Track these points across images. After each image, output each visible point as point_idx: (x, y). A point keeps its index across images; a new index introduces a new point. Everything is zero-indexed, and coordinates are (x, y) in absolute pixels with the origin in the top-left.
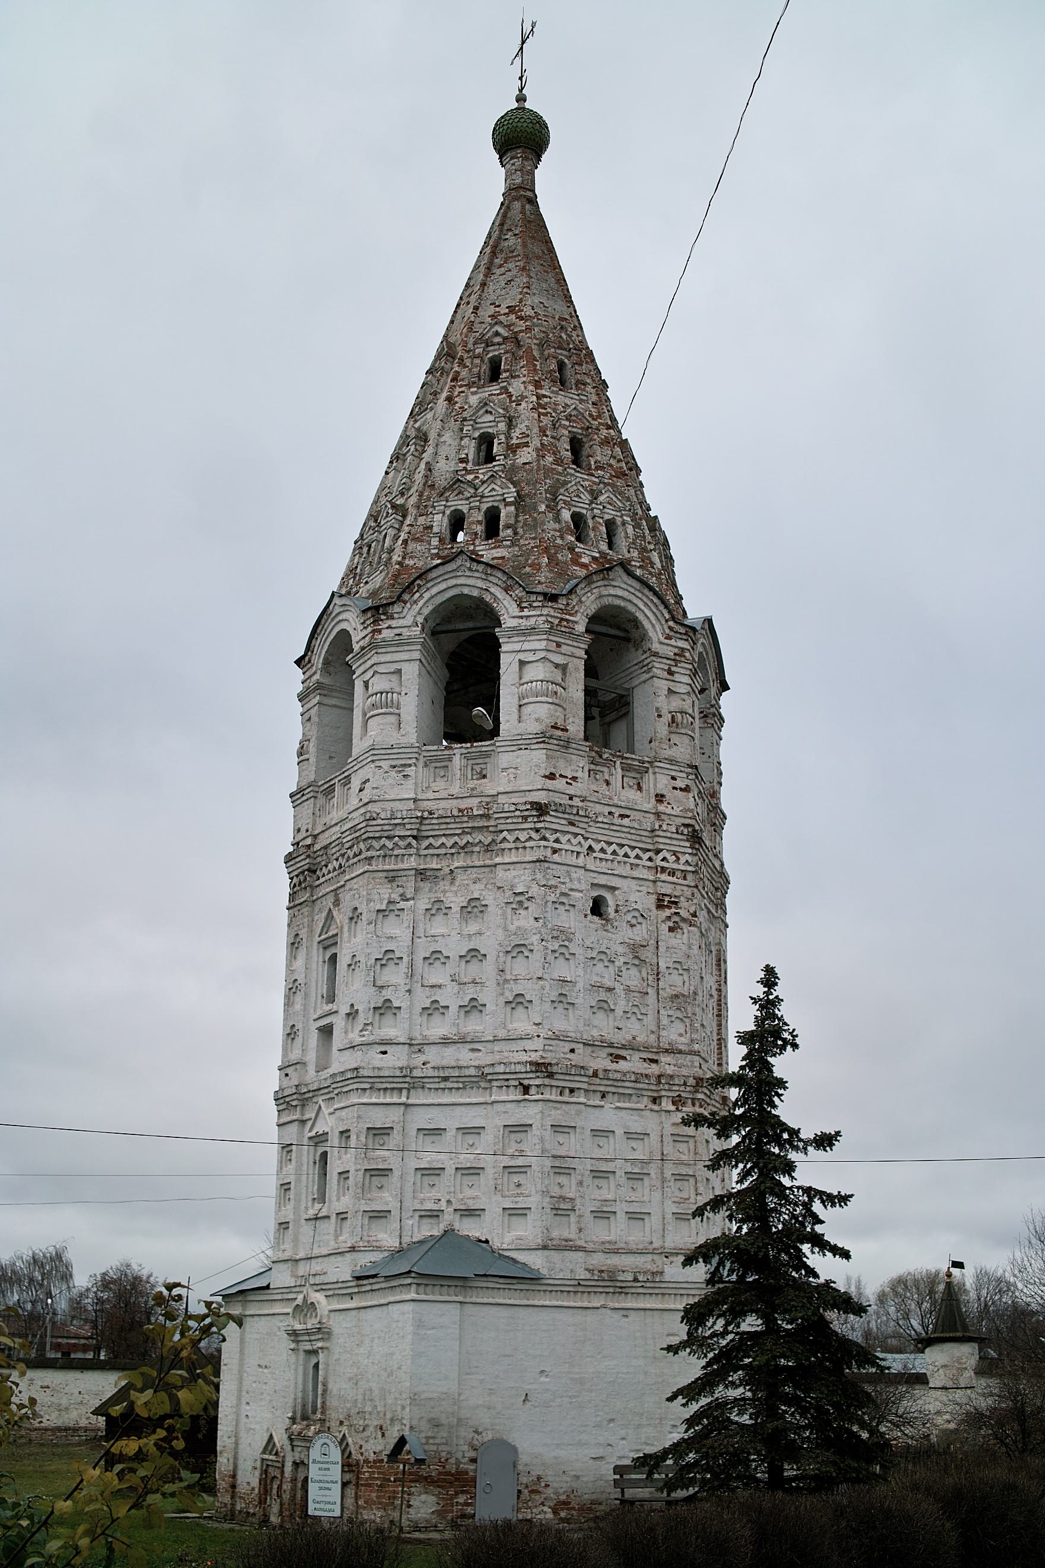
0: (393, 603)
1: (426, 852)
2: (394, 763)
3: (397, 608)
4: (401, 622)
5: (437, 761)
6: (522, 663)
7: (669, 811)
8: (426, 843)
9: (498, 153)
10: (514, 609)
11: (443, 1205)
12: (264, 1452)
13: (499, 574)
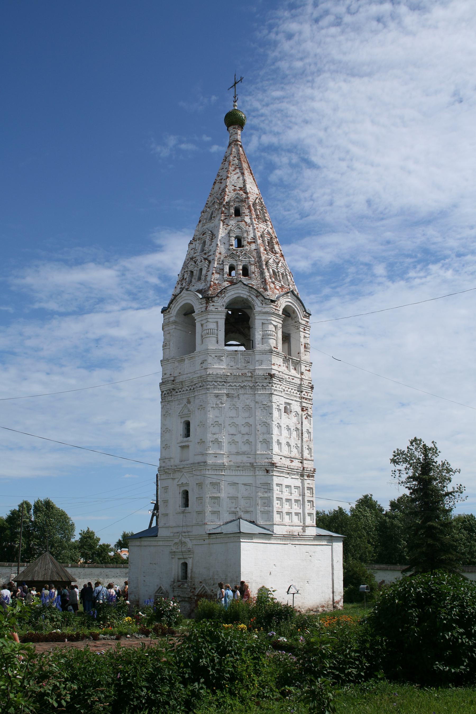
0: (214, 297)
1: (229, 388)
2: (216, 355)
3: (216, 299)
4: (217, 304)
5: (231, 355)
6: (263, 323)
7: (305, 378)
8: (229, 384)
9: (227, 126)
10: (259, 304)
11: (238, 509)
12: (156, 593)
13: (255, 291)
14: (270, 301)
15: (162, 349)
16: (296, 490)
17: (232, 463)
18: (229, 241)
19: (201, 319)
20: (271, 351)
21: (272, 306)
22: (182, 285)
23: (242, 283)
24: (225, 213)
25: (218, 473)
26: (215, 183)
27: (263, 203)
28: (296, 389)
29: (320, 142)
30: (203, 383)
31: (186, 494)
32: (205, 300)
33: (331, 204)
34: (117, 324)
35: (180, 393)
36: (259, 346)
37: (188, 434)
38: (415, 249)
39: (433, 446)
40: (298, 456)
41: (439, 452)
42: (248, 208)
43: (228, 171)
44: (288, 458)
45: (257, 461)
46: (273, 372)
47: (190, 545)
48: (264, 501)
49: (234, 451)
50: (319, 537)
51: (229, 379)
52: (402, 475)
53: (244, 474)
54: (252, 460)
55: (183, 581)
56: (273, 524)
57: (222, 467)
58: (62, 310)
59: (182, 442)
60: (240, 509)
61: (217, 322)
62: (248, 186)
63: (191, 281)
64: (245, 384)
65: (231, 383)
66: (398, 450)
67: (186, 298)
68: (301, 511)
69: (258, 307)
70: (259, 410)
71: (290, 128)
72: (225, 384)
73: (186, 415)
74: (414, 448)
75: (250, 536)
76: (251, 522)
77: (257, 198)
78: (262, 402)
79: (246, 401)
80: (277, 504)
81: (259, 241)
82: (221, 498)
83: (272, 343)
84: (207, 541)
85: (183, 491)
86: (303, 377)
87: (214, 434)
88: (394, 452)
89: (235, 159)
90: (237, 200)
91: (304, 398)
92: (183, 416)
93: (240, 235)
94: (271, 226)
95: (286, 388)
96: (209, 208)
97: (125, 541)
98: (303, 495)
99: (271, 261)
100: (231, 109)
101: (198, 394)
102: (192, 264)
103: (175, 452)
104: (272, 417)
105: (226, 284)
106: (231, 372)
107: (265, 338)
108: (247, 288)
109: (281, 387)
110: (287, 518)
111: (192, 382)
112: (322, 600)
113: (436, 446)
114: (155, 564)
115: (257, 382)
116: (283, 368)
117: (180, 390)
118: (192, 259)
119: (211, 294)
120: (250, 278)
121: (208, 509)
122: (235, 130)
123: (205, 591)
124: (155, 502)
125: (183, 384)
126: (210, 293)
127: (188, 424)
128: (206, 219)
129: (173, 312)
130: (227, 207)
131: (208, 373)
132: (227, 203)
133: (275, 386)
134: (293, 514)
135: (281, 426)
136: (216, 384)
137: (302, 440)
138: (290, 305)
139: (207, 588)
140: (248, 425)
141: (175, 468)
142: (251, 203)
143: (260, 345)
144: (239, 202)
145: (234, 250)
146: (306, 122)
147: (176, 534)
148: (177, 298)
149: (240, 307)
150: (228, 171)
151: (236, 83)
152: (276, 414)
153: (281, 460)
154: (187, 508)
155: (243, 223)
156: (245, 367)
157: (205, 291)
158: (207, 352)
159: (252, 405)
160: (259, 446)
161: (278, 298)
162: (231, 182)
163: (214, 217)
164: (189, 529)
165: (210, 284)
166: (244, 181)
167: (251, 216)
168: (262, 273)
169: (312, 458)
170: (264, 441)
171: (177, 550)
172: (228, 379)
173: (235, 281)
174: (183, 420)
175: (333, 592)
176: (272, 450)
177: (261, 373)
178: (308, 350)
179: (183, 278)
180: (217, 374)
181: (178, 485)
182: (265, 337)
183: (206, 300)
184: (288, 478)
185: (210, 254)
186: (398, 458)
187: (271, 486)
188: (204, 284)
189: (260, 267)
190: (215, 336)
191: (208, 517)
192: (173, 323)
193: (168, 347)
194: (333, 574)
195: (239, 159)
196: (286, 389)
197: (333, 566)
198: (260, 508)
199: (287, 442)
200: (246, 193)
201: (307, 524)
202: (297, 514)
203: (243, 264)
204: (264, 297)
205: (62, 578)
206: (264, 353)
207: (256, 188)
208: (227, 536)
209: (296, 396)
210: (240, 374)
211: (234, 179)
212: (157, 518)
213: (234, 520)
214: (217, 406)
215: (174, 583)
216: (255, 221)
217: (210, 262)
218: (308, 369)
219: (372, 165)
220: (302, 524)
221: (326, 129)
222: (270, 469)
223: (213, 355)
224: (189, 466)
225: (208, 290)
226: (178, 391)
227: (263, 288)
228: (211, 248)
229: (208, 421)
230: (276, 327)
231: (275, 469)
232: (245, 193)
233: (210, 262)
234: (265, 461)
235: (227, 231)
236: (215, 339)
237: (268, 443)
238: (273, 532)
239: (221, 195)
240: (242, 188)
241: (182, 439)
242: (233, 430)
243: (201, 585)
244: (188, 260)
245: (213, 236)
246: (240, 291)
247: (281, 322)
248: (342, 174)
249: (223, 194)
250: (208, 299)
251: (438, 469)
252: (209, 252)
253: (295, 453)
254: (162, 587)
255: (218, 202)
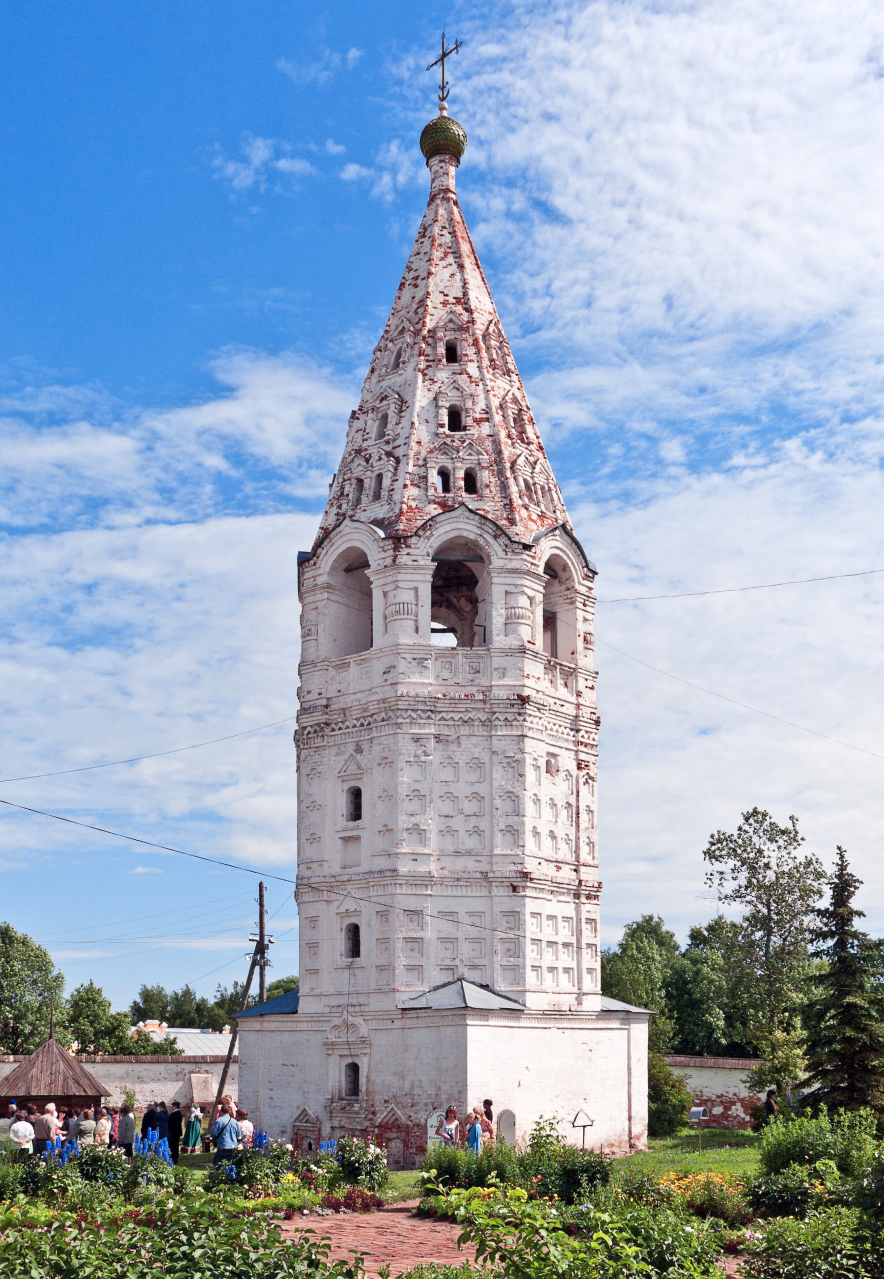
0: (411, 536)
1: (440, 722)
3: (414, 540)
4: (417, 552)
6: (507, 593)
8: (439, 716)
9: (425, 155)
10: (501, 554)
11: (457, 962)
13: (491, 526)
14: (521, 547)
15: (300, 641)
16: (566, 924)
17: (446, 873)
18: (437, 416)
19: (382, 582)
20: (523, 650)
21: (524, 557)
22: (340, 507)
23: (467, 507)
24: (428, 355)
25: (419, 892)
26: (402, 285)
27: (503, 332)
28: (568, 725)
29: (576, 163)
30: (388, 713)
31: (354, 932)
32: (391, 542)
33: (589, 303)
34: (132, 552)
35: (341, 732)
36: (499, 640)
37: (356, 813)
38: (757, 403)
39: (791, 828)
40: (571, 859)
41: (803, 839)
42: (473, 345)
43: (429, 260)
44: (552, 861)
45: (495, 869)
46: (526, 692)
47: (364, 1030)
48: (507, 946)
49: (450, 847)
50: (606, 1013)
51: (440, 706)
52: (725, 883)
53: (469, 894)
54: (484, 867)
55: (349, 1098)
56: (525, 991)
57: (427, 880)
58: (18, 521)
59: (344, 830)
60: (462, 961)
61: (416, 589)
62: (472, 295)
63: (358, 501)
64: (471, 715)
65: (443, 714)
66: (719, 832)
67: (352, 536)
68: (573, 965)
69: (498, 557)
70: (500, 768)
71: (513, 130)
72: (433, 716)
73: (354, 777)
74: (751, 830)
75: (485, 1013)
76: (482, 986)
77: (491, 322)
78: (504, 752)
79: (473, 749)
80: (533, 951)
81: (498, 418)
82: (426, 941)
83: (525, 632)
84: (398, 1024)
85: (349, 925)
86: (581, 701)
87: (412, 815)
88: (712, 836)
89: (445, 232)
90: (451, 325)
91: (582, 743)
92: (346, 778)
93: (458, 403)
94: (518, 384)
95: (549, 723)
96: (392, 341)
97: (149, 1006)
98: (579, 932)
99: (521, 461)
100: (435, 115)
101: (379, 734)
102: (359, 465)
103: (331, 851)
104: (524, 783)
105: (433, 510)
106: (444, 691)
107: (511, 621)
108: (477, 518)
109: (540, 722)
110: (548, 976)
111: (365, 710)
112: (611, 1133)
113: (798, 828)
114: (293, 1065)
115: (495, 713)
116: (544, 685)
117: (340, 725)
118: (358, 451)
119: (404, 530)
120: (481, 497)
121: (401, 961)
122: (443, 164)
123: (394, 1118)
124: (257, 938)
125: (347, 713)
126: (401, 526)
127: (356, 795)
128: (387, 366)
129: (323, 565)
130: (430, 341)
131: (399, 694)
132: (429, 331)
133: (529, 719)
134: (561, 970)
135: (539, 800)
136: (414, 715)
137: (578, 826)
138: (558, 555)
139: (399, 1112)
140: (477, 796)
141: (333, 880)
142: (479, 334)
143: (502, 637)
144: (454, 330)
145: (447, 436)
146: (549, 117)
147: (335, 1010)
148: (331, 536)
149: (461, 558)
150: (429, 260)
151: (444, 55)
152: (530, 775)
153: (539, 867)
154: (358, 959)
155: (465, 376)
156: (472, 681)
157: (390, 524)
158: (396, 649)
159: (485, 757)
160: (499, 838)
161: (537, 540)
162: (436, 285)
163: (404, 363)
164: (362, 1000)
165: (401, 509)
166: (465, 283)
167: (480, 361)
168: (504, 487)
169: (596, 862)
170: (509, 829)
171: (338, 1040)
172: (438, 705)
173: (450, 503)
174: (347, 786)
175: (630, 1118)
176: (524, 846)
177: (503, 694)
178: (590, 647)
179: (342, 494)
180: (417, 696)
181: (337, 914)
182: (510, 621)
183: (394, 543)
184: (550, 900)
185: (397, 443)
186: (718, 849)
187: (521, 916)
188: (386, 507)
189: (501, 473)
190: (412, 617)
191: (401, 976)
192: (324, 588)
193: (314, 637)
194: (629, 1083)
195: (453, 233)
196: (549, 727)
197: (629, 1069)
198: (499, 960)
199: (551, 831)
200: (469, 310)
201: (585, 990)
202: (567, 970)
203: (466, 467)
204: (510, 539)
205: (85, 1091)
206: (509, 652)
207: (488, 299)
208: (440, 1014)
209: (567, 740)
210: (463, 697)
211: (442, 279)
212: (262, 970)
213: (449, 983)
214: (416, 759)
215: (332, 1102)
216: (488, 372)
217: (398, 461)
218: (590, 684)
219: (681, 218)
220: (575, 990)
221: (589, 137)
222: (519, 884)
223: (409, 657)
224: (361, 877)
225: (397, 522)
226: (337, 728)
227: (508, 519)
228: (398, 430)
229: (400, 790)
230: (531, 599)
231: (529, 884)
232: (466, 310)
233: (398, 461)
234: (508, 870)
235: (431, 395)
236: (412, 624)
237: (514, 833)
238: (524, 1005)
239: (416, 313)
240: (460, 299)
241: (346, 823)
242: (447, 808)
243: (386, 1107)
244: (350, 454)
245: (403, 404)
246: (461, 526)
247: (541, 589)
248: (617, 238)
249: (421, 310)
250: (398, 541)
251: (798, 871)
252: (395, 440)
253: (565, 853)
254: (308, 1109)
255: (412, 329)
